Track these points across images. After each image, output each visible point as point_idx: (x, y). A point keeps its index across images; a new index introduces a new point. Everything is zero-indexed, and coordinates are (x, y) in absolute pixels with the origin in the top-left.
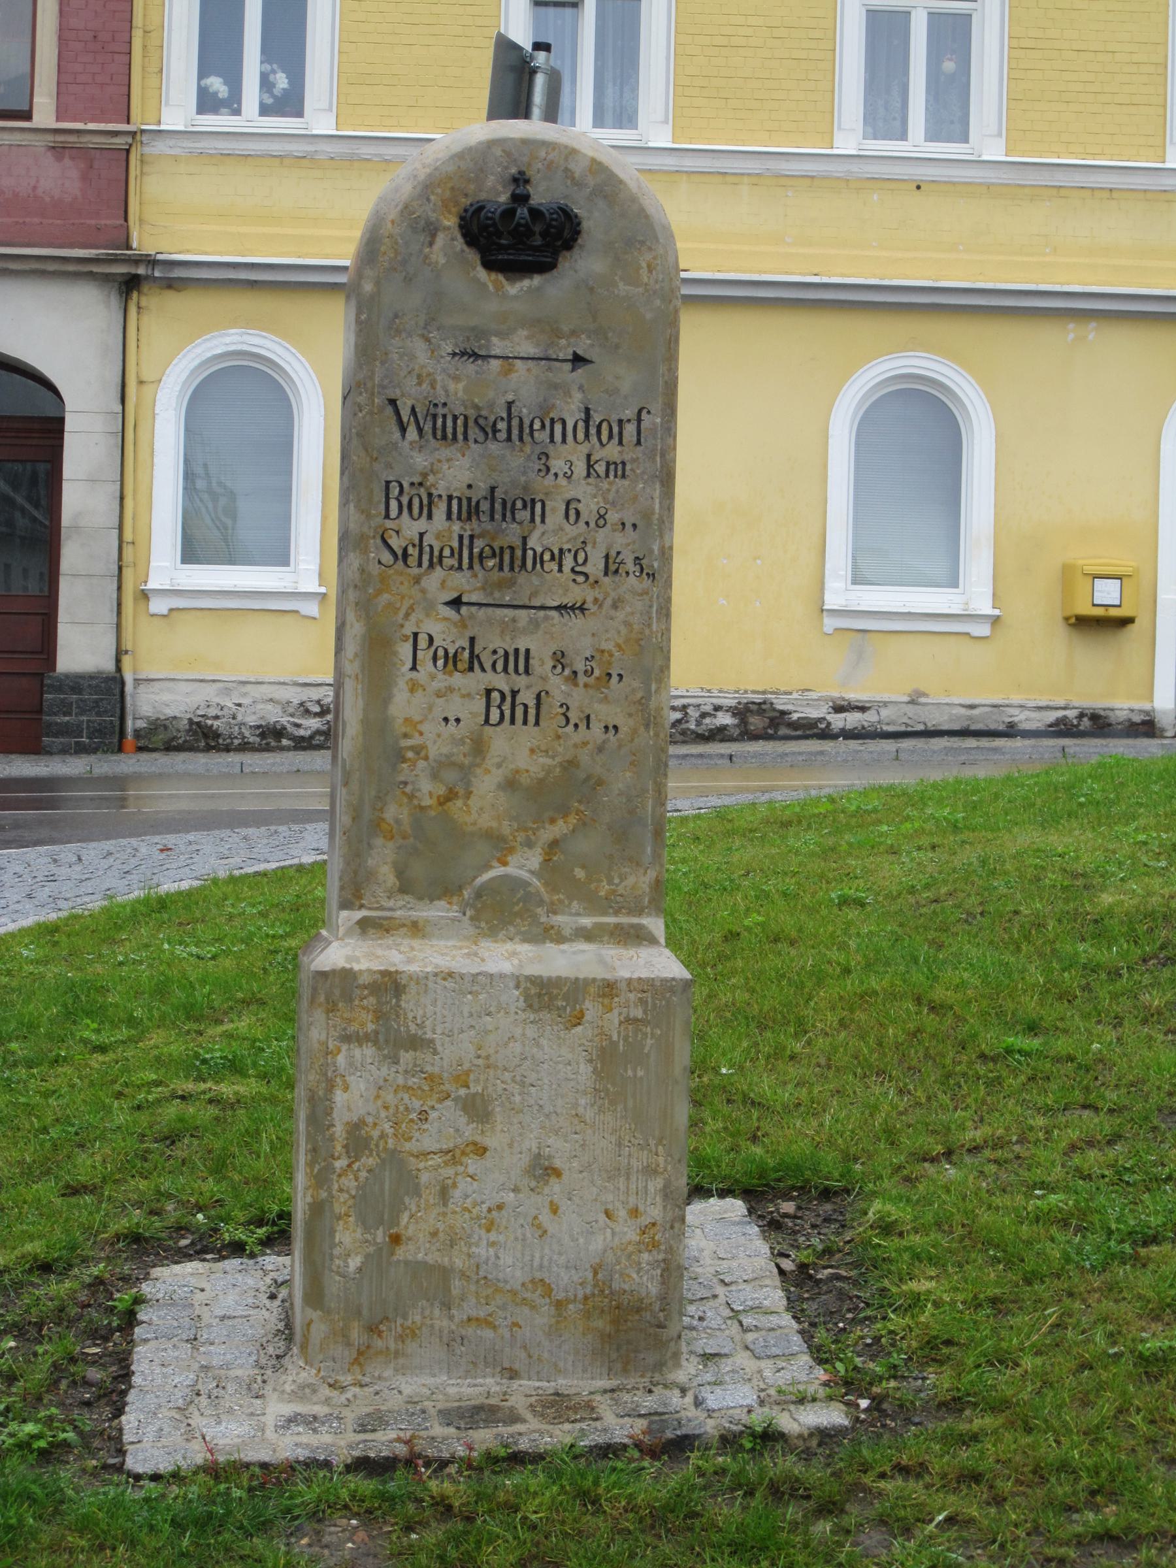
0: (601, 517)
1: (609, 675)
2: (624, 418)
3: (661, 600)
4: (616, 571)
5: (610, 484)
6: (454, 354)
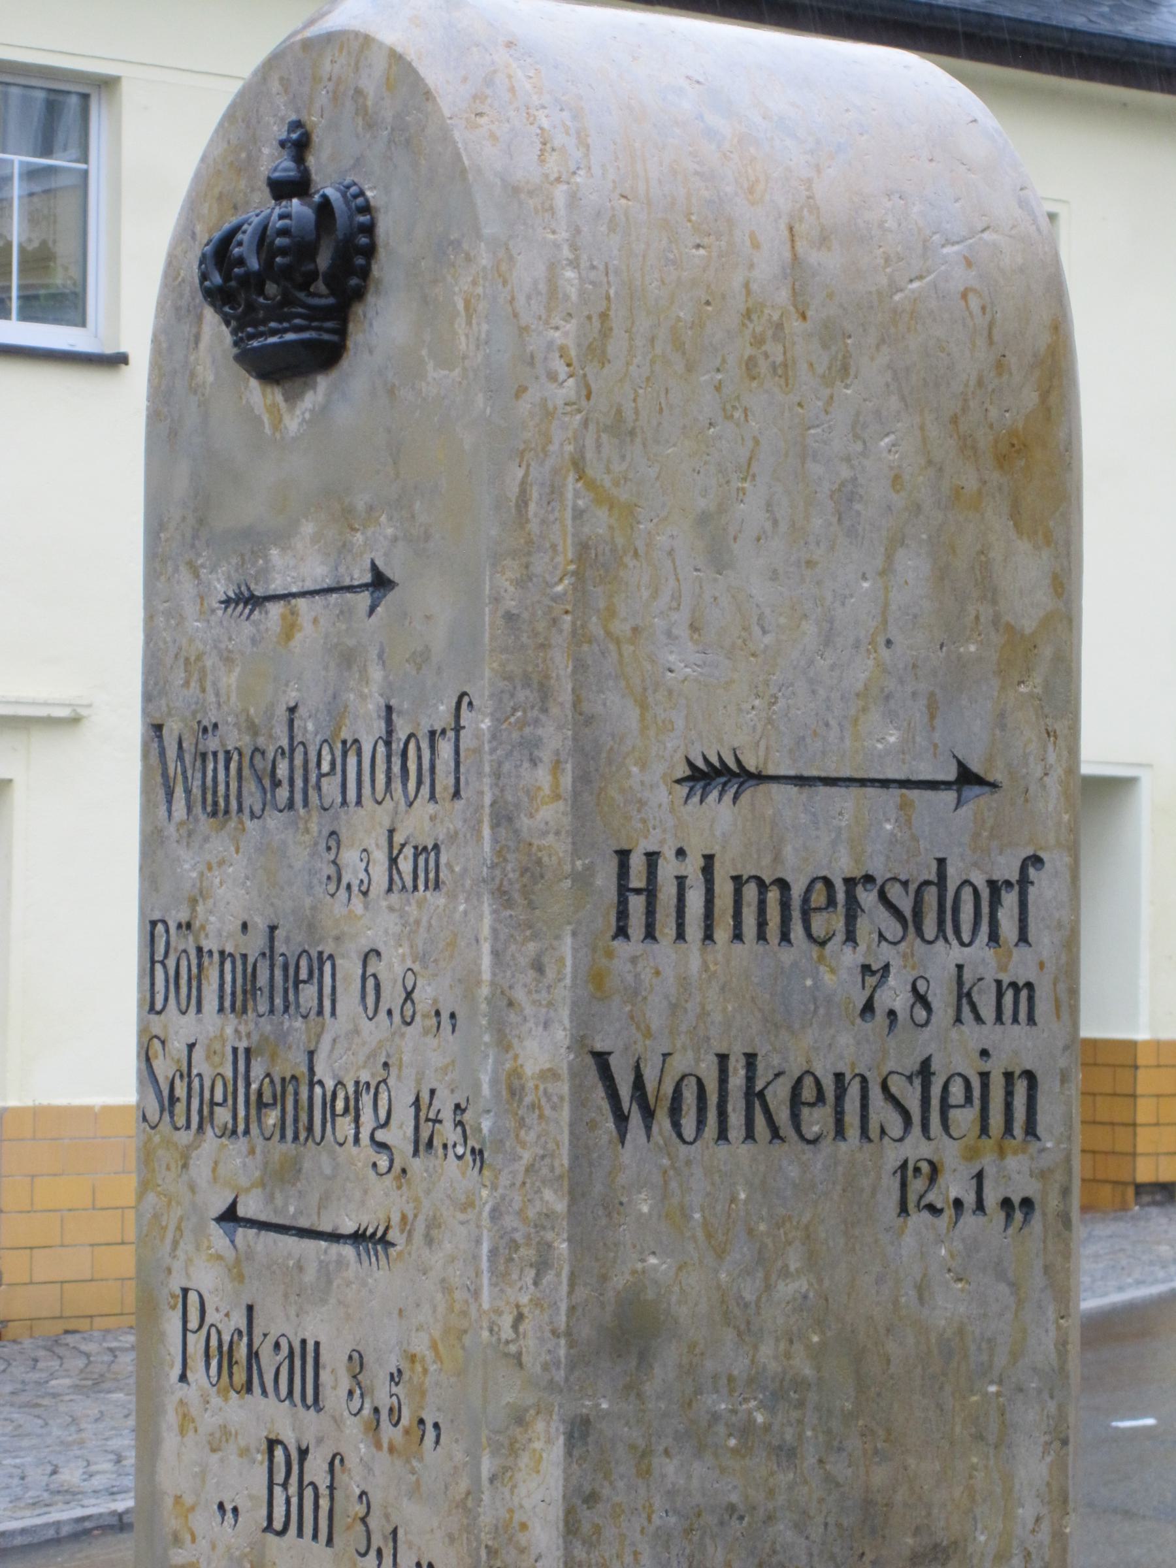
0: (409, 995)
1: (421, 1421)
2: (438, 728)
3: (509, 1221)
4: (430, 1144)
5: (420, 904)
6: (227, 602)
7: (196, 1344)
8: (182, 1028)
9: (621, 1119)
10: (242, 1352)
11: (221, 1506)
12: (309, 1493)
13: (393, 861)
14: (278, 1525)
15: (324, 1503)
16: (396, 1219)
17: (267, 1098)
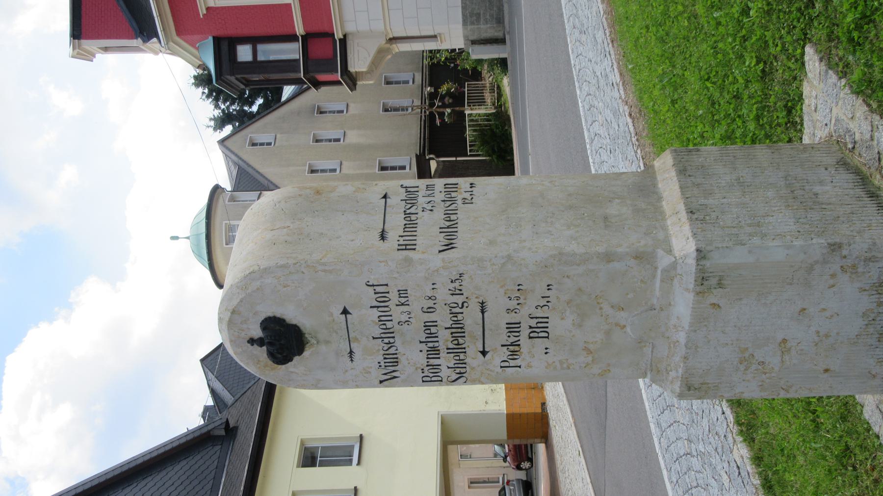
7: (512, 363)
8: (445, 372)
9: (453, 248)
10: (511, 348)
11: (546, 353)
12: (539, 325)
13: (403, 304)
14: (546, 335)
15: (540, 320)
16: (477, 300)
17: (456, 342)
